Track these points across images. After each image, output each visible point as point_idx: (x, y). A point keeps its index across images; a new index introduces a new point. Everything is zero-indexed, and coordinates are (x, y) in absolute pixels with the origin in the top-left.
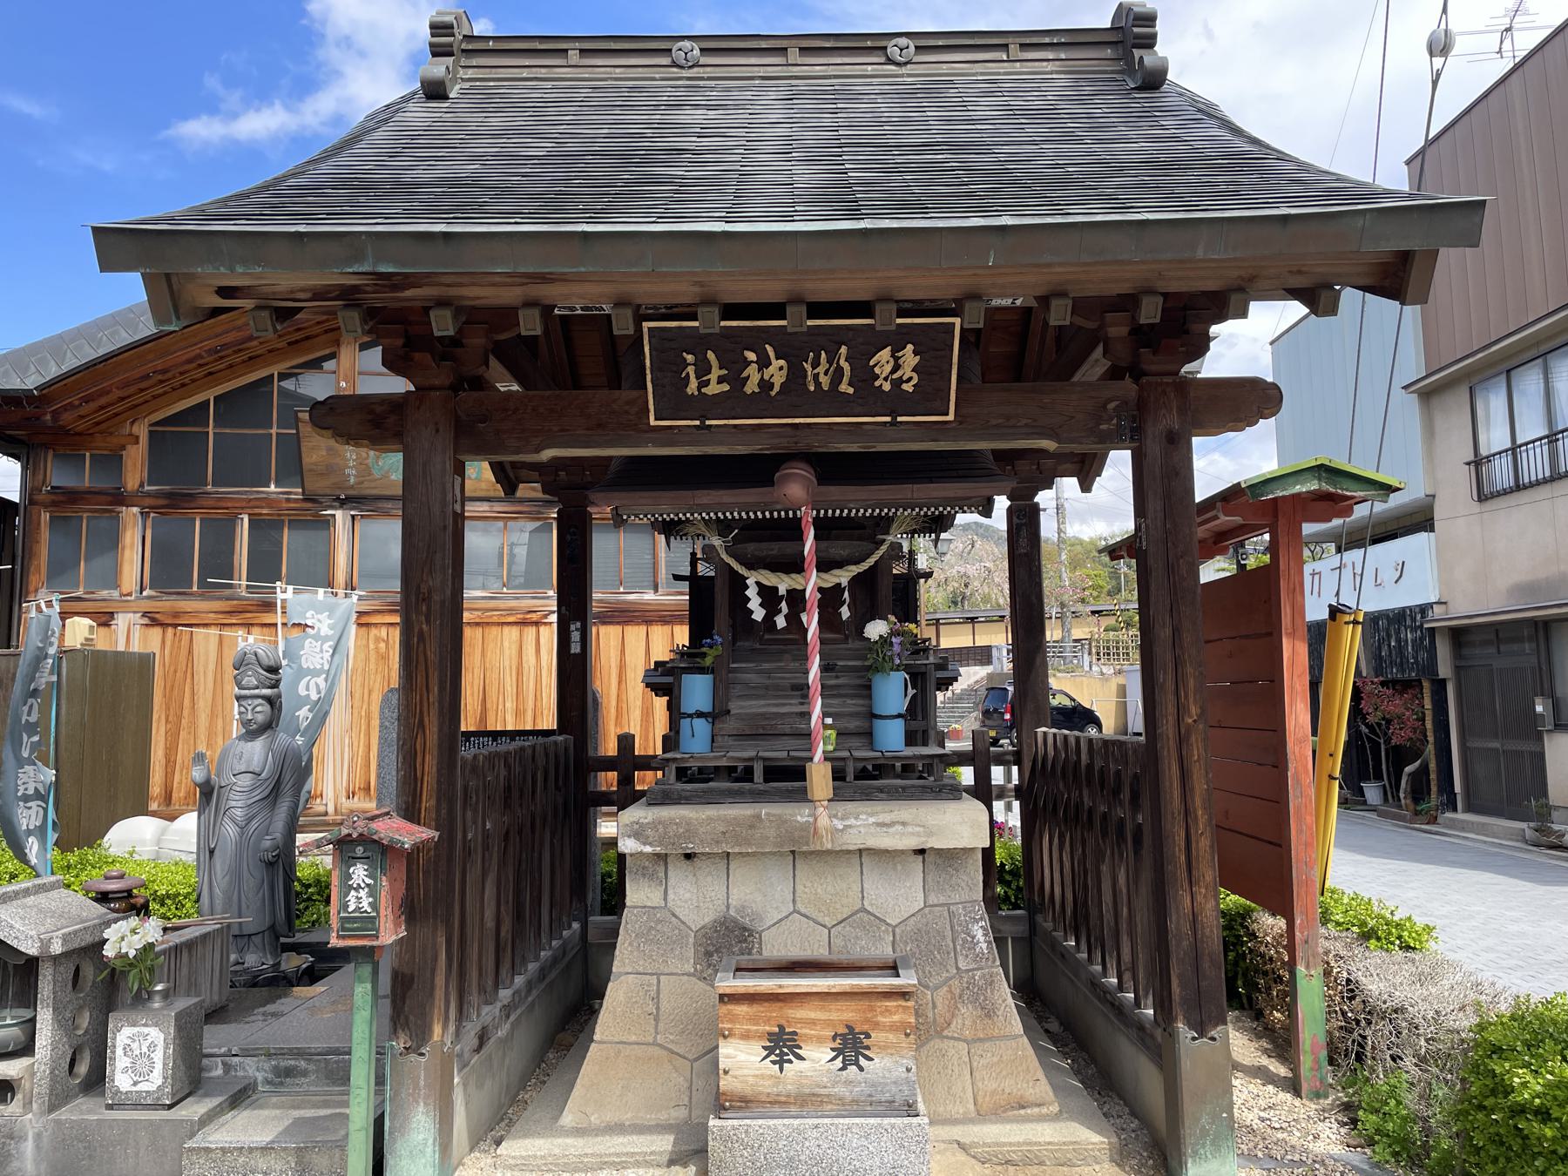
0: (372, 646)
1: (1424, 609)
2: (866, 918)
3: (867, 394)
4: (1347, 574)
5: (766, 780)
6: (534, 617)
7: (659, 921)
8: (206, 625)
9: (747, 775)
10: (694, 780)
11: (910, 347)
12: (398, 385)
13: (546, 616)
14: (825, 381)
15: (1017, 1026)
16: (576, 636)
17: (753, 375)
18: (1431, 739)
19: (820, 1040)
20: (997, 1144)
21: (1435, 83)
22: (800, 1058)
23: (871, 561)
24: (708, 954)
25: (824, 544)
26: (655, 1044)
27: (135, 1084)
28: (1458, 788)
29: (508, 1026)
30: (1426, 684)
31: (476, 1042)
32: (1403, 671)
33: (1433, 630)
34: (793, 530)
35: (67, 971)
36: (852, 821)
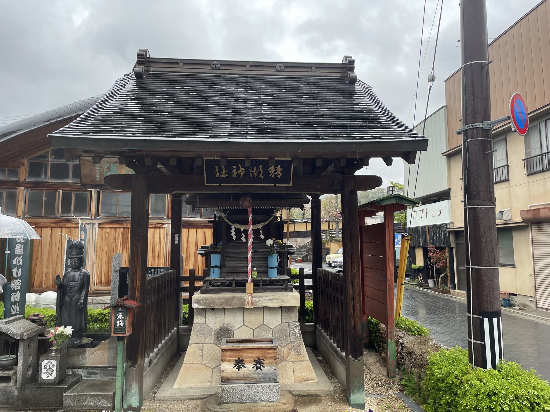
0: (103, 235)
1: (447, 225)
2: (264, 326)
3: (267, 178)
4: (424, 212)
5: (236, 286)
6: (159, 225)
7: (203, 328)
8: (46, 227)
9: (230, 285)
10: (214, 287)
11: (279, 166)
12: (130, 172)
13: (163, 225)
14: (255, 174)
15: (307, 357)
16: (177, 238)
17: (235, 172)
18: (448, 266)
19: (250, 362)
20: (300, 391)
21: (430, 90)
22: (244, 367)
23: (268, 221)
24: (218, 338)
25: (255, 216)
26: (202, 364)
27: (48, 377)
28: (456, 282)
29: (157, 359)
30: (447, 248)
31: (148, 364)
32: (440, 244)
33: (449, 231)
34: (246, 212)
35: (27, 344)
36: (261, 299)
